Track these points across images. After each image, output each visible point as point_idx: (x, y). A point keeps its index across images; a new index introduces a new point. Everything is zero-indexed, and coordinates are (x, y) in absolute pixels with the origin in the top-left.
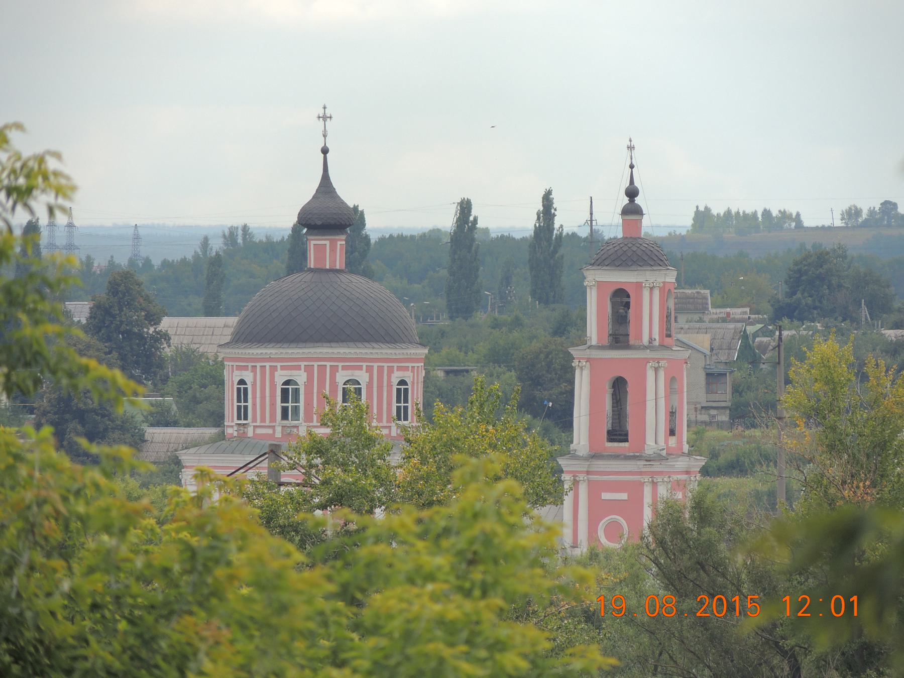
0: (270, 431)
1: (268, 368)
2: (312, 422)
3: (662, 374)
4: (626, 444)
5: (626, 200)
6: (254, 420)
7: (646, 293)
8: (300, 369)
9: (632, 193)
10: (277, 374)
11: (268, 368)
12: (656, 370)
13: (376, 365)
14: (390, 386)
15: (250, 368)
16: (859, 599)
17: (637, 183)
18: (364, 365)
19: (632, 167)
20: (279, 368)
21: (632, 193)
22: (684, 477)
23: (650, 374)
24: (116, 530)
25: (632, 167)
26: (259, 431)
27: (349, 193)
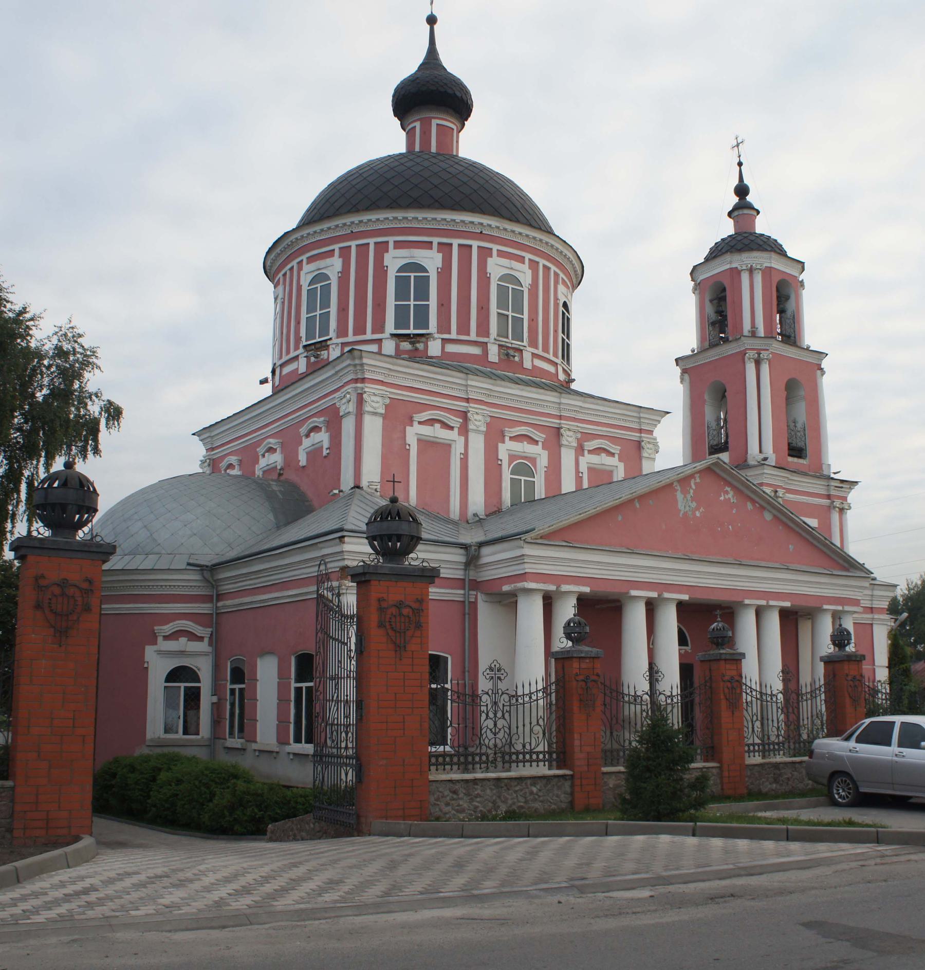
0: (476, 351)
1: (372, 247)
2: (347, 336)
3: (765, 368)
4: (801, 461)
5: (736, 199)
6: (533, 343)
7: (745, 277)
8: (524, 263)
9: (742, 190)
10: (491, 262)
11: (372, 247)
12: (758, 363)
13: (456, 242)
14: (299, 288)
15: (435, 246)
16: (236, 476)
17: (746, 181)
18: (435, 240)
19: (740, 164)
20: (495, 253)
21: (742, 190)
22: (826, 502)
23: (751, 368)
24: (472, 575)
25: (740, 164)
26: (451, 348)
27: (453, 62)
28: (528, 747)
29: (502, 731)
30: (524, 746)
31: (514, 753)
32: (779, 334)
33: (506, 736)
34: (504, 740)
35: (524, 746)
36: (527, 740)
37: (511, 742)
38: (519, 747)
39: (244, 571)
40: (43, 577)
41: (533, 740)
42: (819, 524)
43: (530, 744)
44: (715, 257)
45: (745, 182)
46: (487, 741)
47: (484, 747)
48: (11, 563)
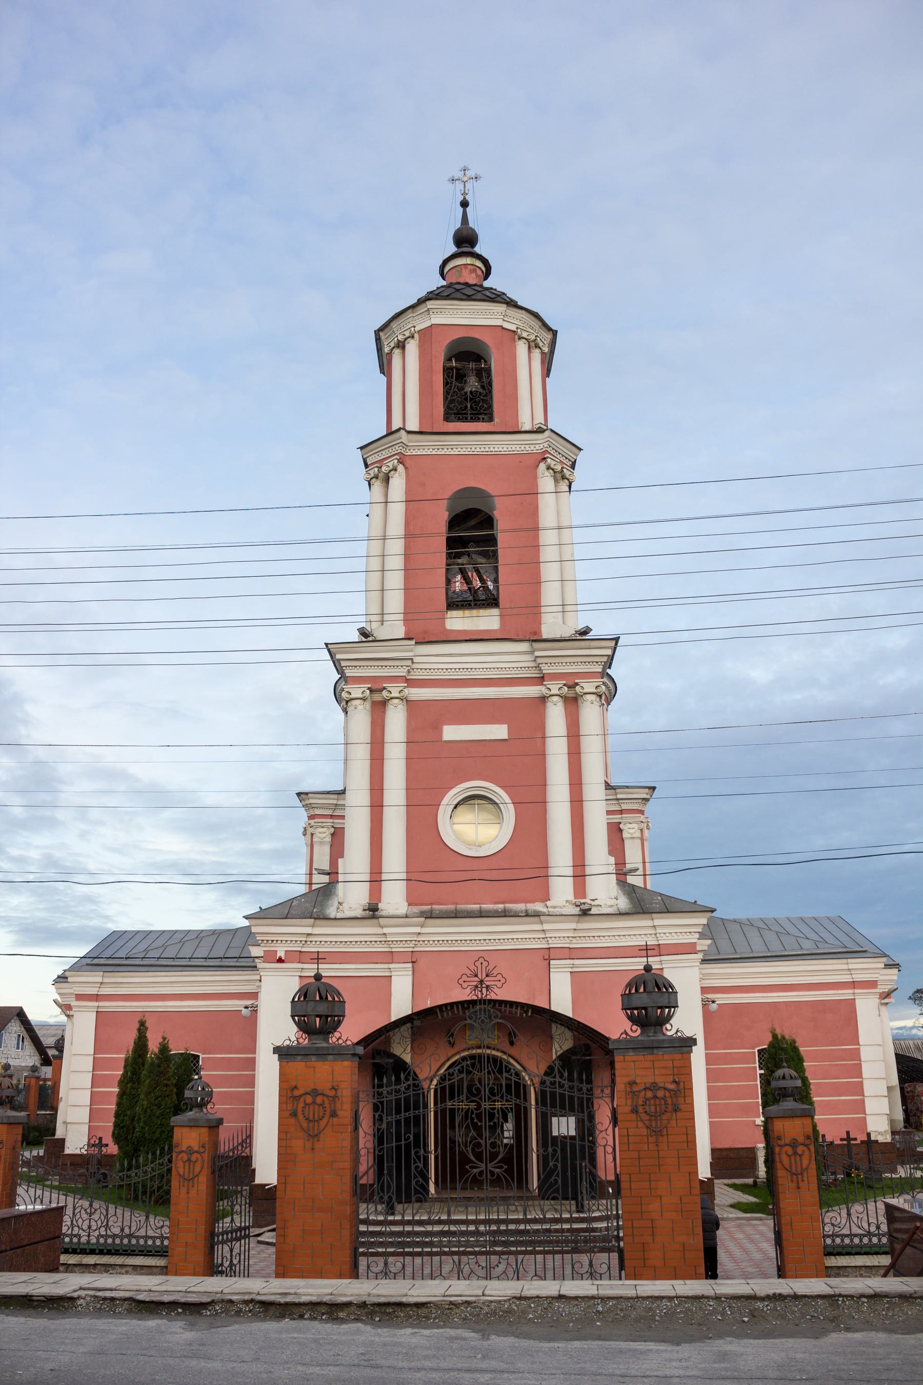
9: (465, 240)
21: (465, 240)
25: (465, 204)
28: (127, 1231)
29: (98, 1211)
30: (122, 1230)
31: (110, 1236)
32: (29, 1172)
33: (102, 1218)
34: (99, 1223)
35: (122, 1230)
36: (126, 1223)
37: (107, 1224)
38: (117, 1231)
39: (158, 980)
40: (635, 1083)
41: (134, 1224)
42: (510, 732)
43: (130, 1228)
44: (447, 297)
45: (471, 225)
46: (80, 1221)
47: (76, 1229)
48: (894, 1171)
